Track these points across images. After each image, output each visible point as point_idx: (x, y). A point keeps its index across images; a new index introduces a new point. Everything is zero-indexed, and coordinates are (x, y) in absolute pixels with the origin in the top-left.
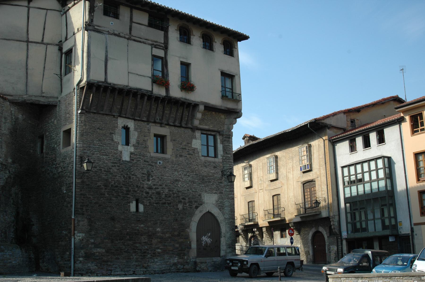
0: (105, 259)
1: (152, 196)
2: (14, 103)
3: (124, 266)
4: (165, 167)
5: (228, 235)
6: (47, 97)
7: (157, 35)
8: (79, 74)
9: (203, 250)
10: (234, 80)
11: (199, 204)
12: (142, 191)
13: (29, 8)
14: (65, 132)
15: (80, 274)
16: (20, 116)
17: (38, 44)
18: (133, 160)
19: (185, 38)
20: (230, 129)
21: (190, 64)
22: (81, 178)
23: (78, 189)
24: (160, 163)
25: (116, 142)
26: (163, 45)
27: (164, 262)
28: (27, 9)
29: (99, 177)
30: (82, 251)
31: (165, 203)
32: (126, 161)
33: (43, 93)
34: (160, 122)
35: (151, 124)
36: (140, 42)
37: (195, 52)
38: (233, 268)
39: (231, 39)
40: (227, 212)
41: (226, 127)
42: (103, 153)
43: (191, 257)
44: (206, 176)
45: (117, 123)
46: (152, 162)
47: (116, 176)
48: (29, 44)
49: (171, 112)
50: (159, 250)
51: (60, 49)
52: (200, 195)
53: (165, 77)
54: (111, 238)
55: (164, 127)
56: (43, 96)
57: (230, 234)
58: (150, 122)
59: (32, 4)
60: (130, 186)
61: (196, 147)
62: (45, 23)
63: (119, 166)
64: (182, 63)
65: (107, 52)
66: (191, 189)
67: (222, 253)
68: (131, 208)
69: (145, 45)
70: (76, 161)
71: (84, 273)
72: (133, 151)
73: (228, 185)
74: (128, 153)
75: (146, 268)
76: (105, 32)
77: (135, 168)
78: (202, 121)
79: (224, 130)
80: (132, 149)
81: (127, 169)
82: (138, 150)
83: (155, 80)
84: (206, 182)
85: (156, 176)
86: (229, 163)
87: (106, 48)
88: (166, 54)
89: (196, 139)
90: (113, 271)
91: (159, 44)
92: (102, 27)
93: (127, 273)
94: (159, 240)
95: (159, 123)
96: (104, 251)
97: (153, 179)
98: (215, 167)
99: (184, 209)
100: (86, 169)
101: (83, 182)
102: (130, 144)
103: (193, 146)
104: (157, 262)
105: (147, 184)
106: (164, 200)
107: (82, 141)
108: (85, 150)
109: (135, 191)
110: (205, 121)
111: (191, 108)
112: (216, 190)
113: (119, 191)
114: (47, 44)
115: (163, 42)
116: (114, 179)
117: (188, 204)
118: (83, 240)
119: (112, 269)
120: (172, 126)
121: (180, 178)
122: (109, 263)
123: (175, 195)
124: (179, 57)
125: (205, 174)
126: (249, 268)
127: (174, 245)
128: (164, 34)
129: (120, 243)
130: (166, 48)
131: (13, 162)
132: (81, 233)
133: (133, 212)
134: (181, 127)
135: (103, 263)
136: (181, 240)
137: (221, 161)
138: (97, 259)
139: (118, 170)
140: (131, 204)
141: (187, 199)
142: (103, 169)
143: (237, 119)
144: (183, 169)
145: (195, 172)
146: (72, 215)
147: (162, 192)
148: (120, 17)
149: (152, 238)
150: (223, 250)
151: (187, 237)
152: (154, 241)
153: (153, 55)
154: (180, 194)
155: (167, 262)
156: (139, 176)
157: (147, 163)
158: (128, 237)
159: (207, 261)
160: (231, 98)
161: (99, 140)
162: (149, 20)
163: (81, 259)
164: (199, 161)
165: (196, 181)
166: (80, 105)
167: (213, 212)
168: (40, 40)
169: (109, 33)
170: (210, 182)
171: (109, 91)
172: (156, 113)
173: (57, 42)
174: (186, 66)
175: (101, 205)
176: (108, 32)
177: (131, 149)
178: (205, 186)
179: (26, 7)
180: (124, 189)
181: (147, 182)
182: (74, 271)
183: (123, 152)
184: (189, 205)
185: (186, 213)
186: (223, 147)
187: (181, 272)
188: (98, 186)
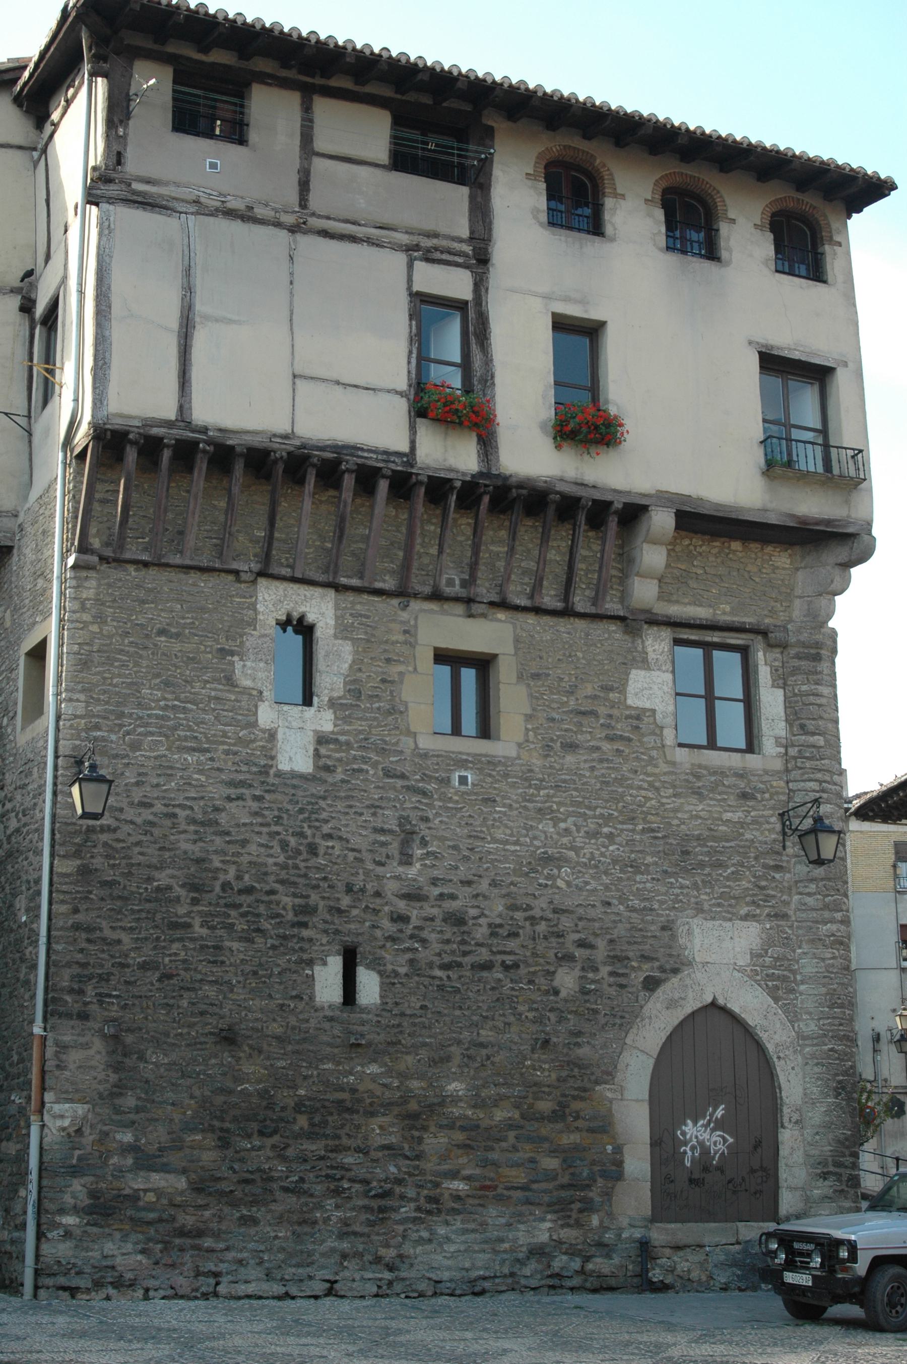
0: (188, 1220)
1: (425, 934)
3: (281, 1256)
4: (490, 801)
5: (816, 1116)
7: (441, 205)
8: (74, 402)
9: (686, 1190)
10: (832, 391)
11: (662, 969)
12: (376, 912)
14: (29, 654)
15: (64, 1288)
18: (328, 769)
19: (576, 202)
20: (819, 618)
21: (602, 325)
22: (77, 854)
23: (63, 902)
24: (463, 780)
25: (246, 691)
26: (467, 249)
27: (486, 1242)
31: (487, 966)
32: (294, 775)
34: (463, 593)
35: (416, 605)
37: (627, 268)
38: (790, 1278)
39: (808, 204)
40: (810, 1005)
41: (798, 610)
42: (186, 739)
43: (624, 1222)
44: (698, 838)
45: (253, 607)
46: (425, 778)
47: (244, 843)
49: (512, 550)
50: (459, 1186)
51: (27, 308)
53: (477, 387)
54: (216, 1123)
55: (484, 616)
57: (827, 1113)
58: (415, 596)
60: (316, 887)
61: (648, 705)
63: (257, 798)
64: (562, 325)
65: (188, 290)
66: (622, 900)
67: (788, 1202)
68: (318, 987)
69: (375, 249)
70: (55, 777)
71: (83, 1282)
73: (812, 880)
74: (308, 740)
75: (391, 1268)
76: (180, 207)
77: (340, 806)
79: (791, 621)
80: (326, 722)
81: (301, 811)
82: (358, 725)
83: (427, 405)
84: (702, 865)
85: (442, 839)
86: (819, 776)
87: (188, 272)
88: (480, 286)
89: (648, 668)
90: (224, 1280)
91: (444, 243)
92: (166, 184)
93: (294, 1291)
94: (459, 1137)
95: (457, 599)
96: (182, 1183)
98: (744, 796)
99: (584, 992)
101: (85, 872)
102: (315, 700)
103: (629, 702)
104: (448, 1240)
105: (396, 877)
106: (484, 950)
107: (83, 691)
108: (97, 727)
109: (340, 911)
110: (693, 584)
113: (262, 909)
115: (465, 233)
116: (239, 854)
117: (604, 971)
118: (79, 1131)
119: (223, 1267)
120: (525, 609)
121: (563, 846)
122: (208, 1242)
123: (542, 927)
124: (547, 297)
125: (695, 828)
126: (865, 1282)
127: (532, 1161)
128: (472, 198)
129: (260, 1148)
130: (480, 260)
132: (71, 1101)
134: (567, 612)
135: (177, 1241)
136: (569, 1139)
137: (778, 765)
138: (149, 1223)
139: (256, 814)
140: (317, 969)
141: (601, 944)
142: (182, 814)
143: (853, 570)
144: (579, 804)
146: (32, 1022)
147: (473, 912)
148: (253, 136)
149: (425, 1128)
150: (790, 1188)
151: (603, 1126)
152: (435, 1142)
153: (418, 294)
154: (566, 922)
155: (501, 1240)
156: (356, 841)
157: (400, 783)
158: (302, 1121)
159: (706, 1241)
160: (820, 469)
161: (167, 684)
162: (396, 140)
163: (69, 1220)
164: (664, 767)
166: (74, 534)
169: (200, 208)
170: (720, 865)
171: (201, 465)
172: (441, 551)
173: (13, 279)
174: (579, 337)
175: (170, 977)
176: (197, 202)
178: (695, 886)
180: (288, 901)
181: (401, 869)
182: (37, 1273)
183: (280, 736)
184: (611, 974)
185: (596, 1012)
186: (788, 704)
187: (572, 1289)
188: (158, 889)
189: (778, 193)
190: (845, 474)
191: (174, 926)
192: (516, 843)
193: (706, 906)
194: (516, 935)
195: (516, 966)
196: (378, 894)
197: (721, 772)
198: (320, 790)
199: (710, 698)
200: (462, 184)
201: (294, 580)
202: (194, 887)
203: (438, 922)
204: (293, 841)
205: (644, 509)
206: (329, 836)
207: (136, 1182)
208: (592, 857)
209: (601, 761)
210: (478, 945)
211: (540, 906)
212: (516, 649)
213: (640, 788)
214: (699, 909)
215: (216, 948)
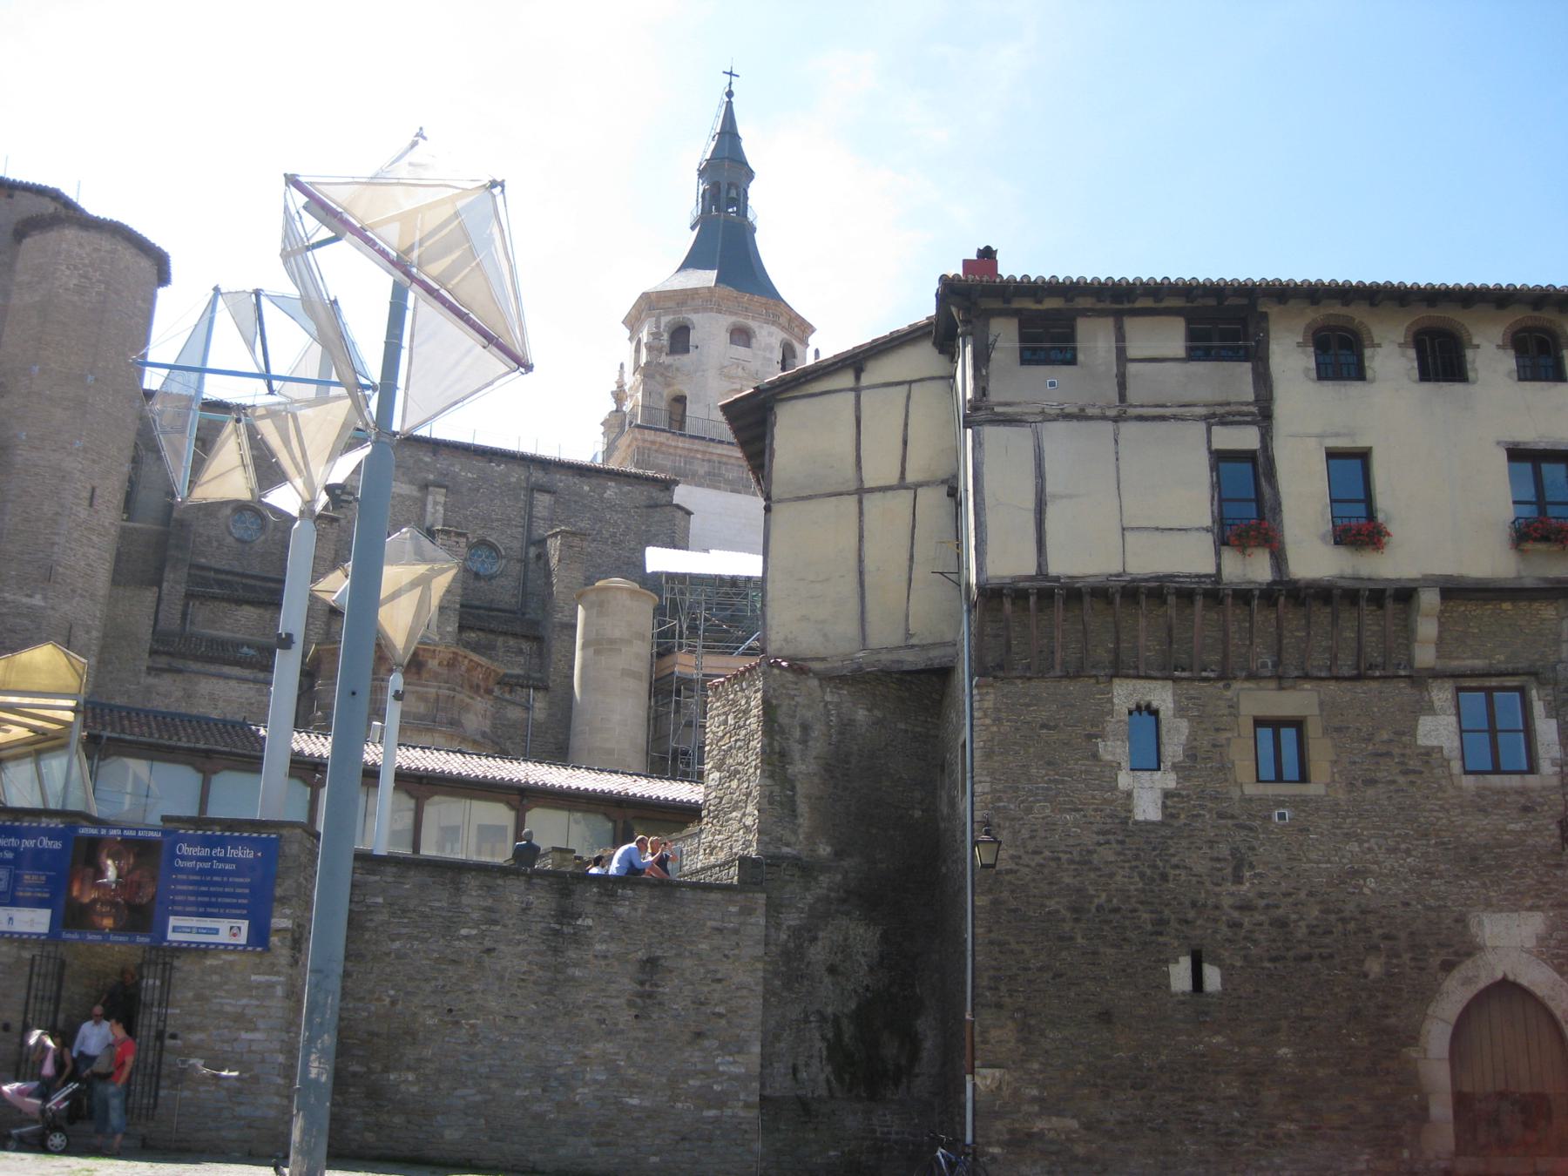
1: (1257, 935)
2: (832, 679)
4: (1304, 831)
6: (923, 647)
7: (1236, 381)
11: (1456, 953)
12: (1216, 921)
13: (857, 390)
16: (861, 714)
17: (889, 494)
18: (1172, 816)
19: (1340, 355)
22: (990, 891)
24: (1282, 816)
25: (1109, 764)
26: (1254, 409)
29: (1051, 883)
30: (999, 1125)
31: (1308, 958)
32: (1147, 823)
33: (912, 636)
36: (1163, 418)
45: (1110, 701)
46: (1251, 816)
52: (1461, 920)
53: (1268, 514)
54: (1099, 1081)
55: (1293, 688)
56: (913, 646)
59: (865, 380)
61: (1435, 743)
62: (906, 425)
63: (1122, 842)
69: (1180, 424)
74: (1157, 796)
77: (1184, 843)
80: (1169, 780)
85: (1266, 863)
88: (1266, 436)
91: (1234, 408)
97: (1256, 875)
98: (1526, 809)
99: (1389, 974)
101: (996, 903)
105: (1228, 895)
108: (1000, 799)
109: (1187, 922)
112: (1537, 896)
113: (1127, 923)
114: (916, 487)
115: (1251, 397)
117: (1406, 957)
123: (1352, 926)
128: (1254, 370)
130: (1264, 416)
131: (839, 854)
133: (1184, 993)
137: (1555, 781)
139: (1119, 854)
140: (1171, 967)
142: (1064, 857)
145: (1437, 836)
146: (964, 1010)
147: (1294, 917)
148: (1081, 357)
153: (1218, 451)
156: (1198, 869)
157: (1230, 822)
161: (1049, 763)
162: (1191, 336)
163: (996, 1150)
165: (1442, 867)
167: (1524, 982)
168: (894, 479)
170: (1505, 866)
174: (1351, 466)
175: (1061, 976)
179: (851, 389)
180: (1146, 916)
183: (1135, 795)
184: (1412, 959)
185: (1400, 990)
191: (1061, 938)
192: (1329, 861)
193: (1494, 901)
194: (1331, 932)
195: (1331, 956)
196: (1217, 907)
197: (1503, 792)
198: (1168, 832)
199: (1493, 731)
200: (1246, 360)
201: (1138, 677)
202: (1074, 910)
203: (1266, 926)
204: (1148, 872)
205: (1415, 589)
206: (1176, 867)
207: (1039, 1125)
208: (1393, 869)
209: (1397, 791)
210: (1300, 942)
211: (1350, 908)
212: (1322, 710)
213: (1432, 810)
214: (1489, 905)
215: (1094, 953)
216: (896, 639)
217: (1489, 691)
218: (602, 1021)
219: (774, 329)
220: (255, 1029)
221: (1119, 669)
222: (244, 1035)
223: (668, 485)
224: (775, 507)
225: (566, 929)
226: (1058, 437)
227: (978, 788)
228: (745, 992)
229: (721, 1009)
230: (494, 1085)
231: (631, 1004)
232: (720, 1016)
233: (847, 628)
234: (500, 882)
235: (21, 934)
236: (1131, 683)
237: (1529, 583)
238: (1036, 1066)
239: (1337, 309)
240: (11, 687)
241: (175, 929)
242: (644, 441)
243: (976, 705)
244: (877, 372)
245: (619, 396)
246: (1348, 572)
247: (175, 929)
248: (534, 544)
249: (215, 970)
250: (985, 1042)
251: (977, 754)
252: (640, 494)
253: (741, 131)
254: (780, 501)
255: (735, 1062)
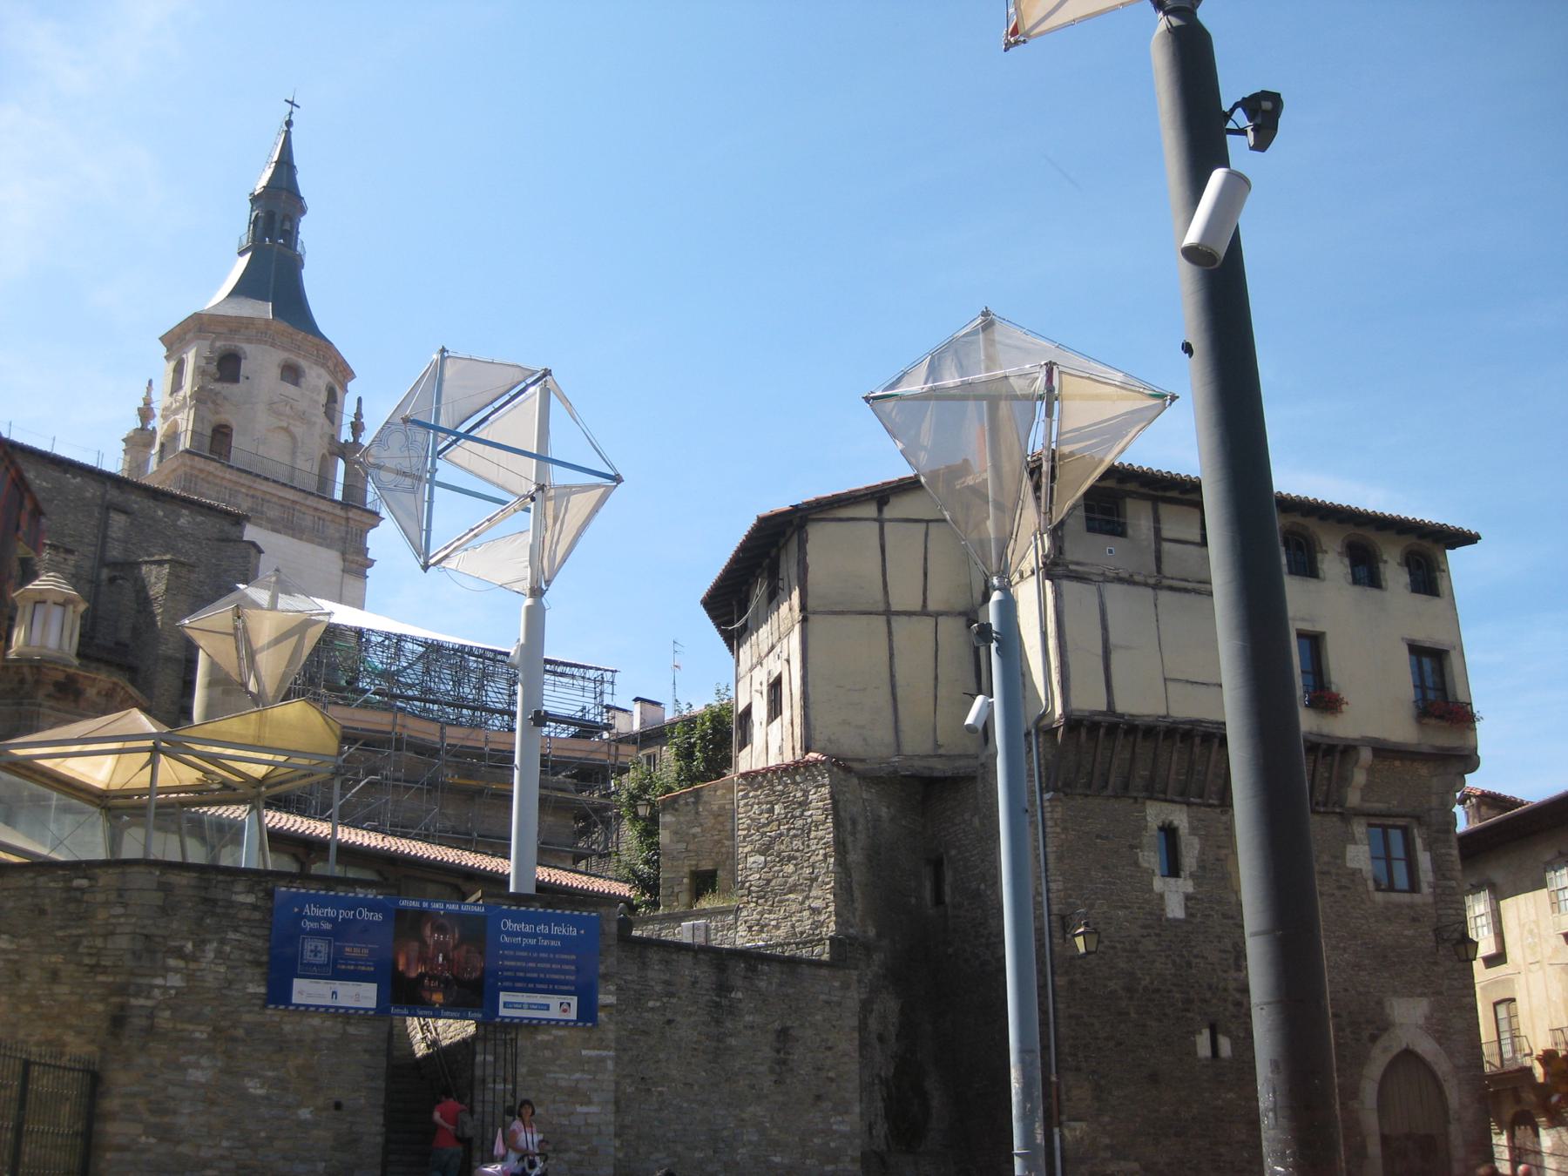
6: (948, 757)
13: (881, 522)
16: (884, 811)
17: (914, 618)
25: (1146, 870)
28: (876, 525)
32: (1176, 920)
36: (1186, 590)
39: (1424, 551)
48: (894, 619)
52: (1380, 1003)
59: (888, 512)
63: (1158, 935)
72: (1190, 890)
76: (1095, 578)
78: (1368, 789)
100: (1082, 950)
101: (1072, 983)
111: (1338, 757)
114: (937, 615)
117: (1348, 1030)
137: (1430, 900)
148: (1130, 532)
167: (1419, 1050)
168: (918, 607)
176: (1103, 574)
177: (1185, 885)
186: (1434, 861)
189: (1410, 540)
190: (1462, 717)
197: (1399, 906)
201: (1166, 801)
206: (1196, 956)
216: (926, 747)
217: (1385, 828)
218: (752, 1087)
219: (322, 371)
220: (590, 1103)
221: (1154, 791)
222: (579, 1109)
223: (238, 520)
224: (811, 617)
225: (724, 1002)
226: (1114, 591)
227: (1053, 886)
228: (846, 1059)
229: (831, 1074)
230: (679, 1148)
231: (772, 1071)
232: (831, 1080)
233: (882, 734)
234: (674, 957)
235: (347, 1008)
236: (1158, 805)
237: (1425, 749)
238: (1106, 1119)
239: (1299, 519)
240: (266, 743)
241: (506, 1005)
242: (192, 467)
243: (1048, 815)
244: (896, 509)
245: (146, 413)
246: (1315, 729)
247: (506, 1005)
248: (107, 565)
249: (546, 1046)
250: (1069, 1100)
251: (1051, 858)
252: (212, 526)
253: (297, 161)
254: (815, 613)
255: (842, 1122)
